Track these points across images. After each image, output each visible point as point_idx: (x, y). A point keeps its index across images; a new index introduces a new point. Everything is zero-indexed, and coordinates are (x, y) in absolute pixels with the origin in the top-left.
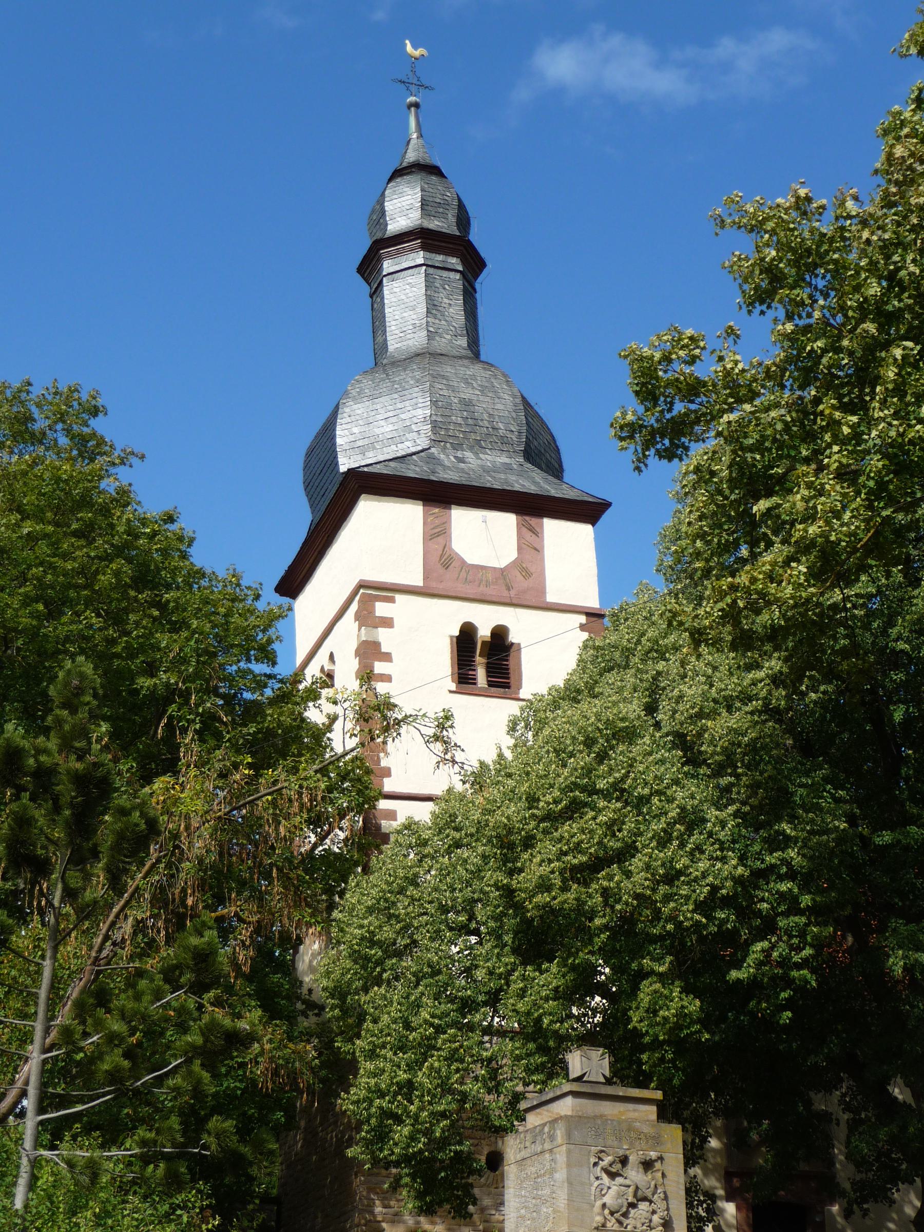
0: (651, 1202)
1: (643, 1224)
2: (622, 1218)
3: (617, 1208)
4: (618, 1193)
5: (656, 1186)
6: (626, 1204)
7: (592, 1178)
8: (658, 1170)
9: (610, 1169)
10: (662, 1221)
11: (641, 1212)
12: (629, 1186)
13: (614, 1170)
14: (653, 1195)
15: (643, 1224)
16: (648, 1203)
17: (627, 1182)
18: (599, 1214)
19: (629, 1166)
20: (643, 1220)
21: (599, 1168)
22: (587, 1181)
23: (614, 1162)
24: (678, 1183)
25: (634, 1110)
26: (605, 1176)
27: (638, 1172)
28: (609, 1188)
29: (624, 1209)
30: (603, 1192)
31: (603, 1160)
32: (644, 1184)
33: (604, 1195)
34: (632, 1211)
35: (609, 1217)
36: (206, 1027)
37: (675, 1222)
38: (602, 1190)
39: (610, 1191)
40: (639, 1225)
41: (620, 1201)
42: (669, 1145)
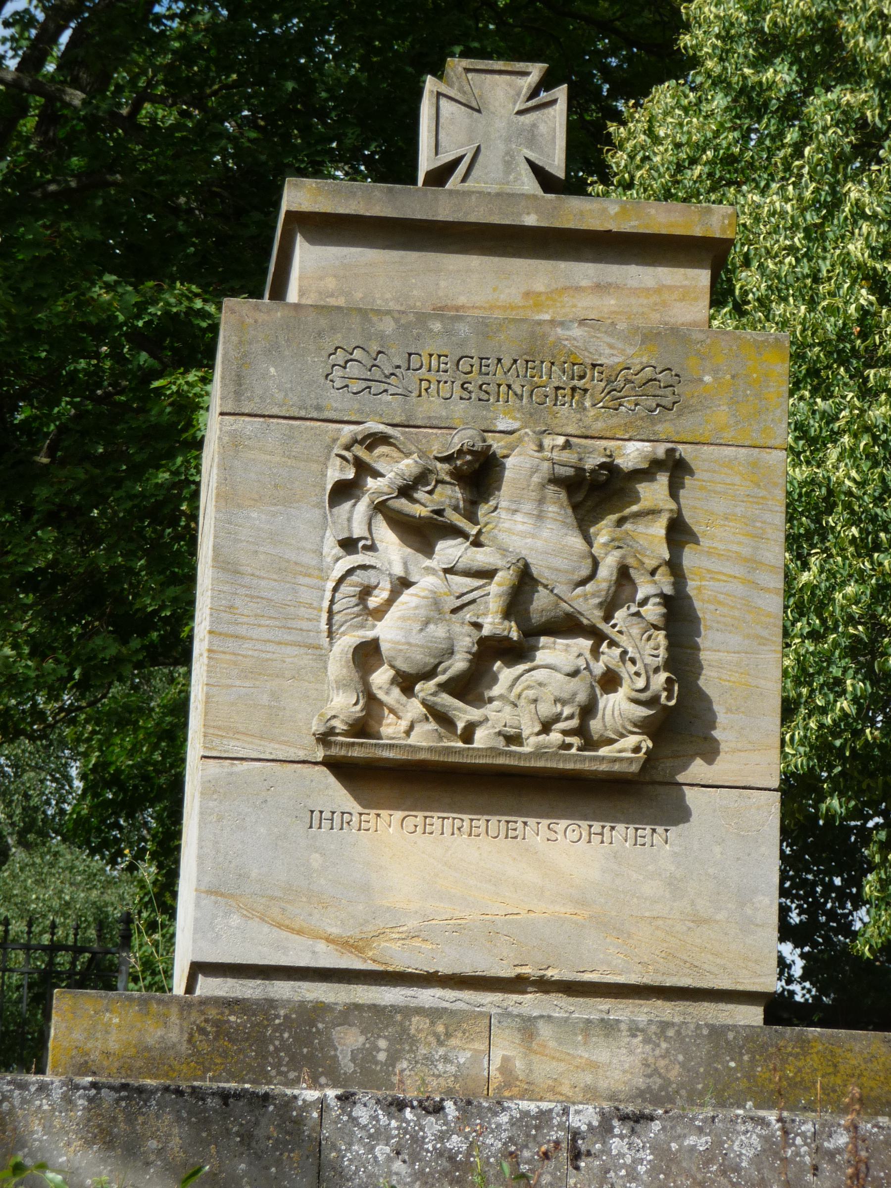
0: (597, 636)
1: (546, 727)
2: (446, 699)
3: (420, 659)
4: (436, 603)
5: (624, 574)
6: (466, 642)
7: (331, 548)
8: (653, 512)
9: (402, 504)
10: (643, 712)
11: (540, 675)
12: (487, 574)
13: (419, 511)
14: (609, 609)
15: (546, 727)
16: (585, 644)
17: (482, 557)
18: (341, 685)
19: (504, 496)
20: (546, 709)
21: (362, 506)
22: (309, 559)
23: (421, 478)
24: (753, 563)
25: (600, 288)
26: (386, 536)
27: (540, 517)
28: (404, 584)
29: (459, 664)
30: (373, 602)
31: (376, 474)
32: (560, 563)
33: (379, 613)
34: (506, 674)
35: (393, 697)
36: (555, 345)
37: (722, 717)
38: (366, 591)
39: (407, 597)
40: (529, 727)
41: (438, 631)
42: (721, 413)
